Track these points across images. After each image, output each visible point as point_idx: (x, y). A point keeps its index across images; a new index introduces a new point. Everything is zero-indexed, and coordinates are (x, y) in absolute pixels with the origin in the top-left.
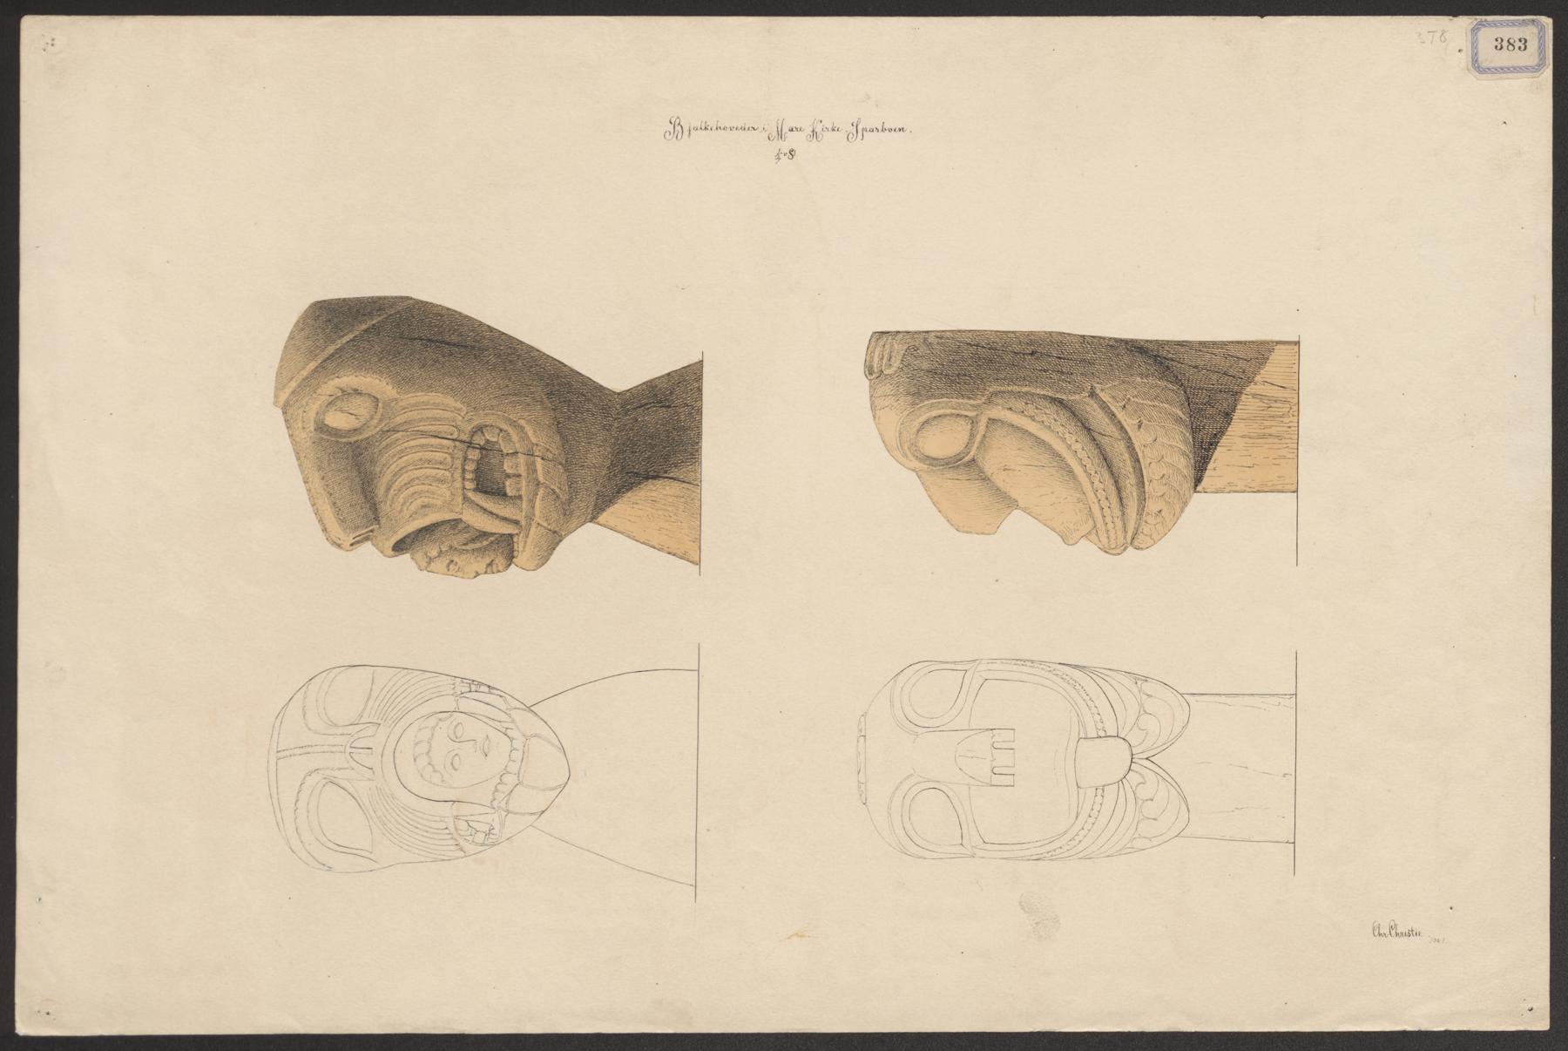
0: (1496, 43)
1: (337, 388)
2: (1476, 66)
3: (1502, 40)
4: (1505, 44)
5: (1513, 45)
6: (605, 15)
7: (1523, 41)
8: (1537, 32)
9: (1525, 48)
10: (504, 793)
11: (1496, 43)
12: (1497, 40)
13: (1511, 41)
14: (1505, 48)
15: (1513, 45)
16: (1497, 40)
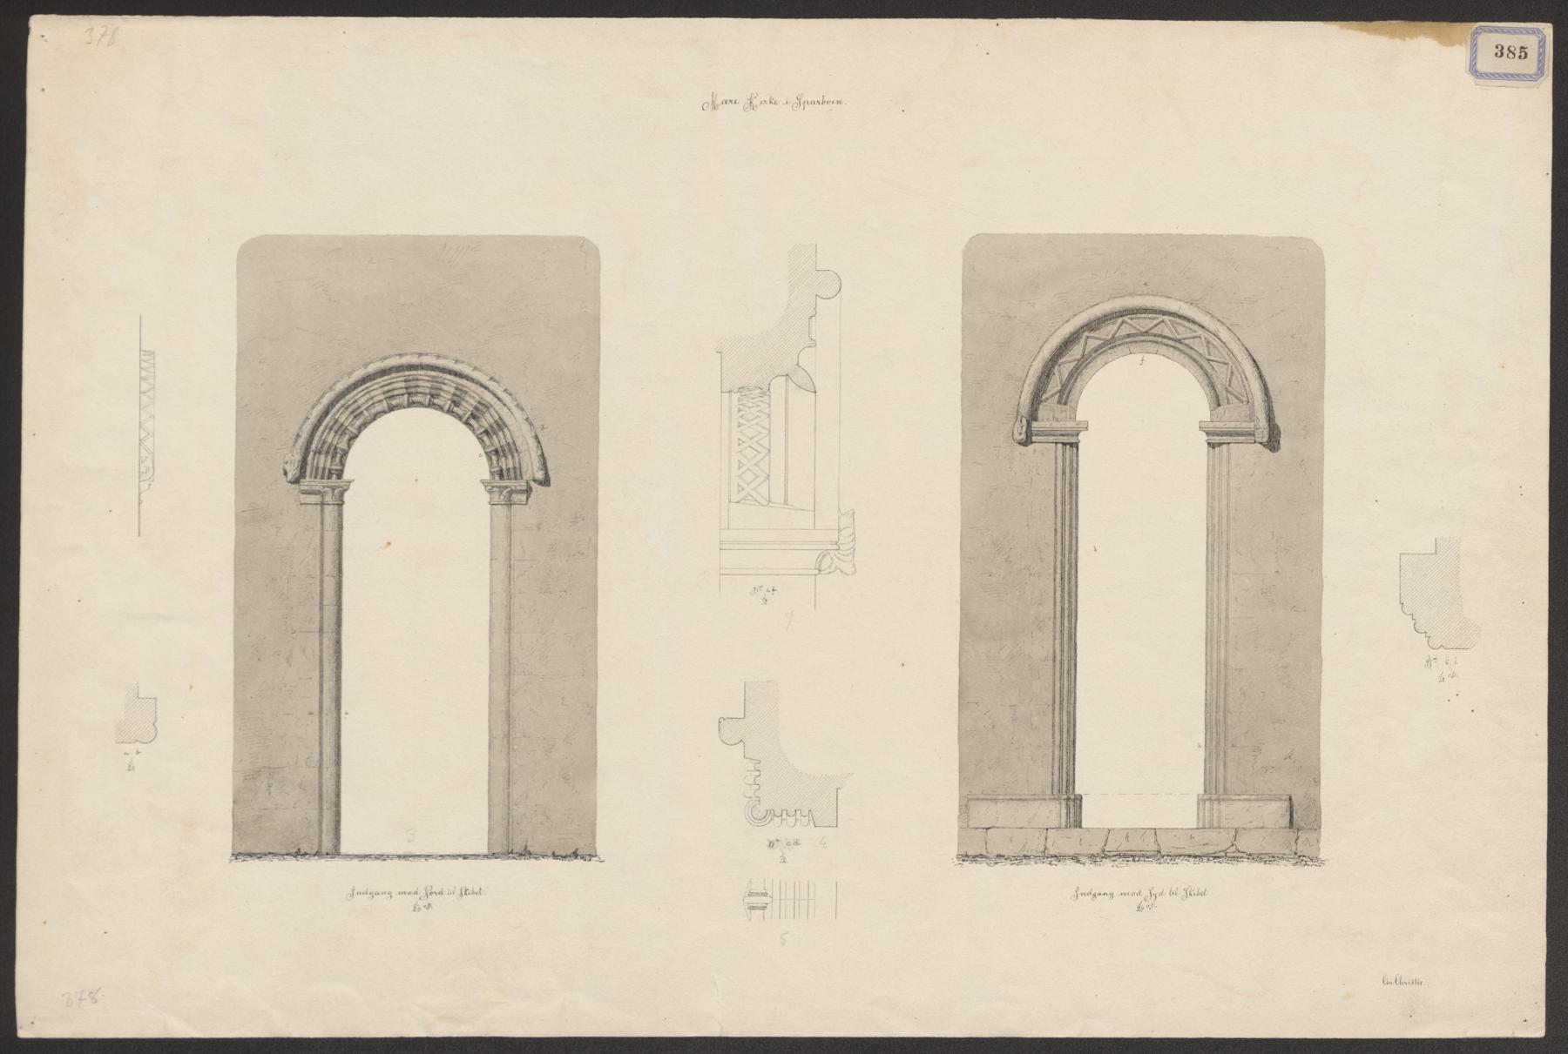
0: (1496, 50)
1: (353, 480)
2: (1473, 70)
3: (1502, 48)
4: (1506, 51)
5: (1514, 54)
6: (199, 1040)
7: (1500, 49)
8: (1538, 36)
9: (1526, 57)
10: (1209, 354)
11: (1496, 50)
12: (1497, 47)
13: (1512, 49)
14: (1505, 55)
15: (1514, 54)
16: (1497, 47)
